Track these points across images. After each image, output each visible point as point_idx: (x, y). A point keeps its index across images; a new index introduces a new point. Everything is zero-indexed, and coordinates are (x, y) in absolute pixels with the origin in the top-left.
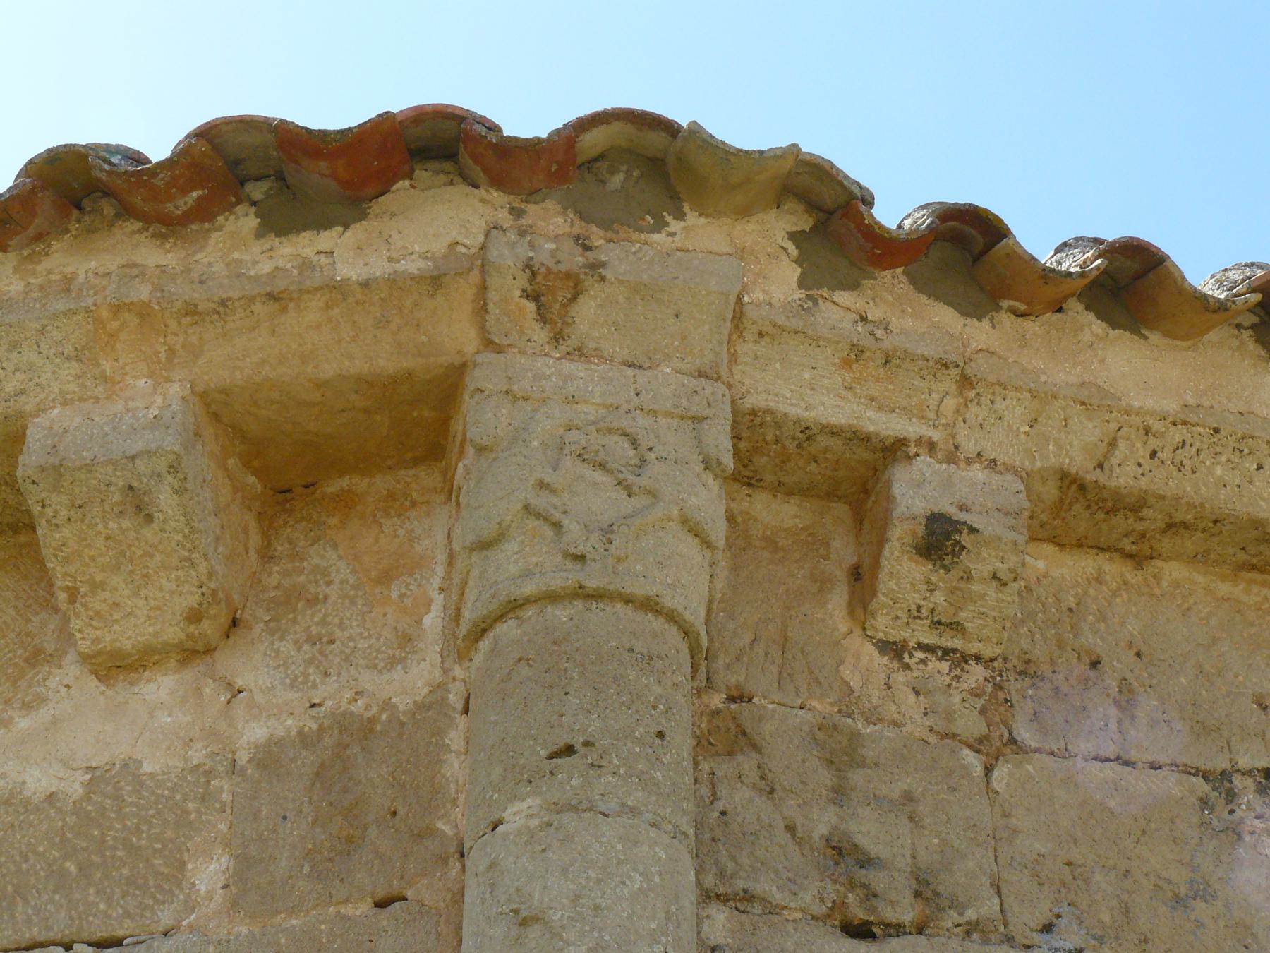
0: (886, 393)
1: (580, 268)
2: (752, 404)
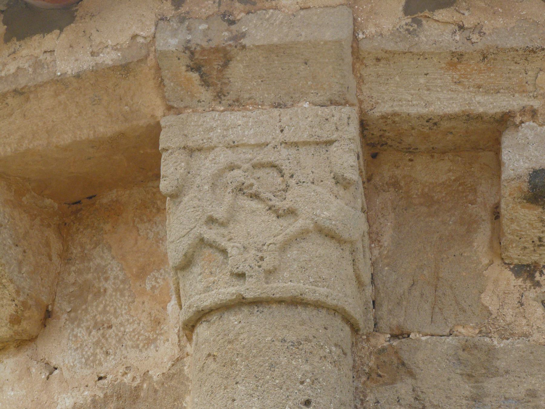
1: (226, 41)
2: (381, 112)
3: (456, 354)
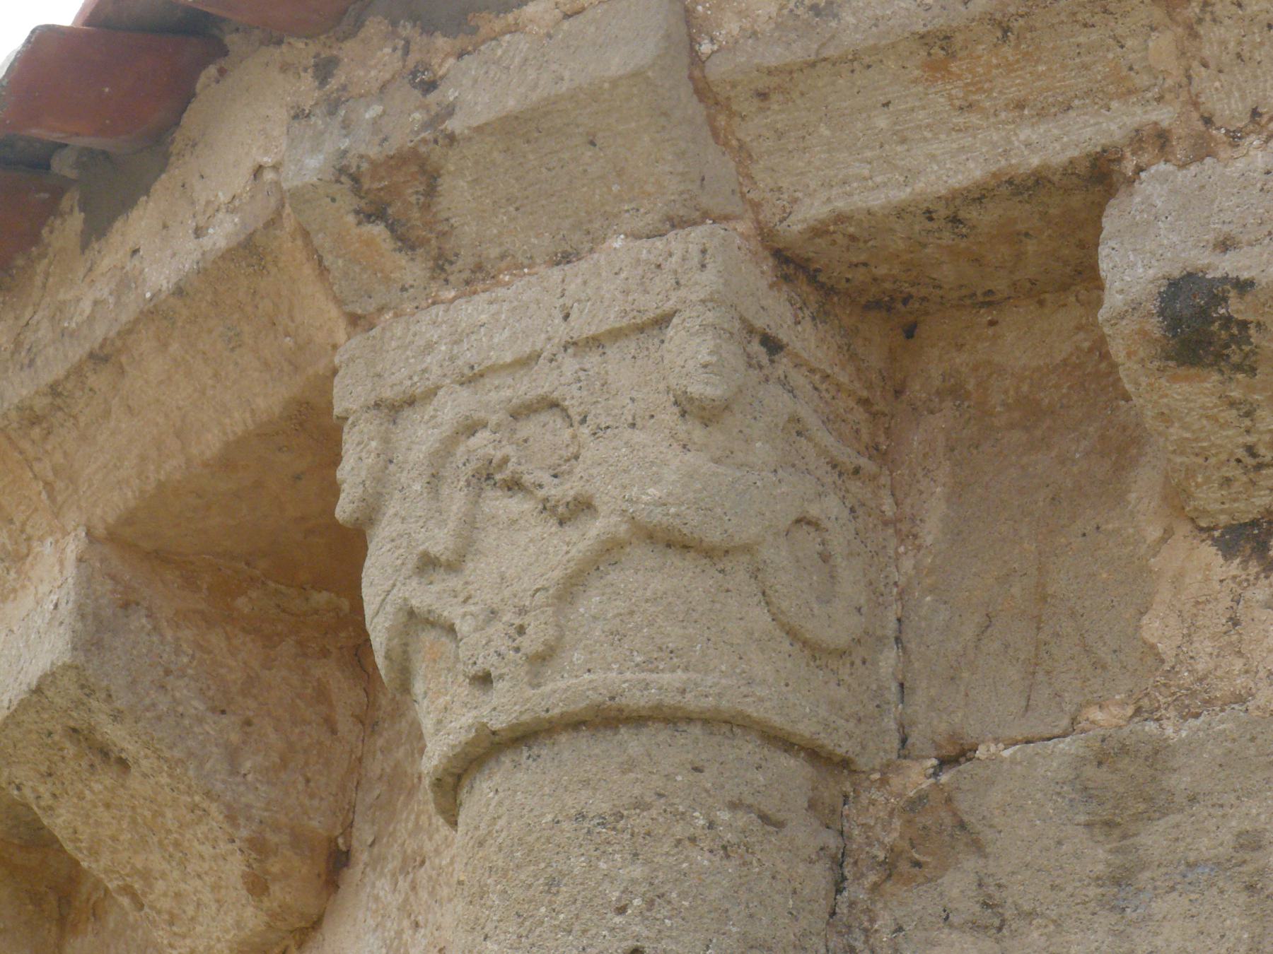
0: (1038, 84)
1: (418, 133)
2: (805, 220)
3: (1077, 777)
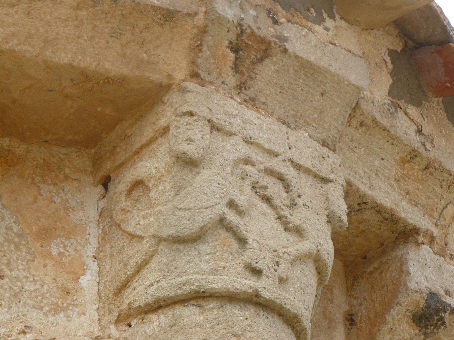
0: (416, 191)
